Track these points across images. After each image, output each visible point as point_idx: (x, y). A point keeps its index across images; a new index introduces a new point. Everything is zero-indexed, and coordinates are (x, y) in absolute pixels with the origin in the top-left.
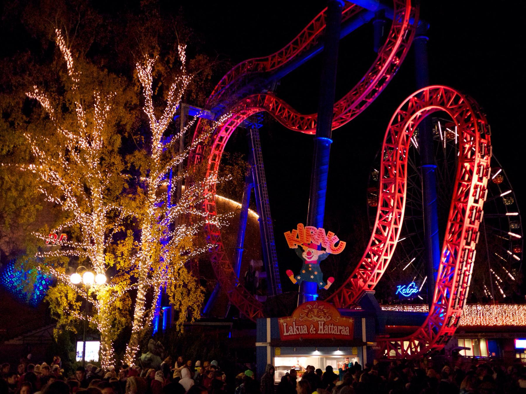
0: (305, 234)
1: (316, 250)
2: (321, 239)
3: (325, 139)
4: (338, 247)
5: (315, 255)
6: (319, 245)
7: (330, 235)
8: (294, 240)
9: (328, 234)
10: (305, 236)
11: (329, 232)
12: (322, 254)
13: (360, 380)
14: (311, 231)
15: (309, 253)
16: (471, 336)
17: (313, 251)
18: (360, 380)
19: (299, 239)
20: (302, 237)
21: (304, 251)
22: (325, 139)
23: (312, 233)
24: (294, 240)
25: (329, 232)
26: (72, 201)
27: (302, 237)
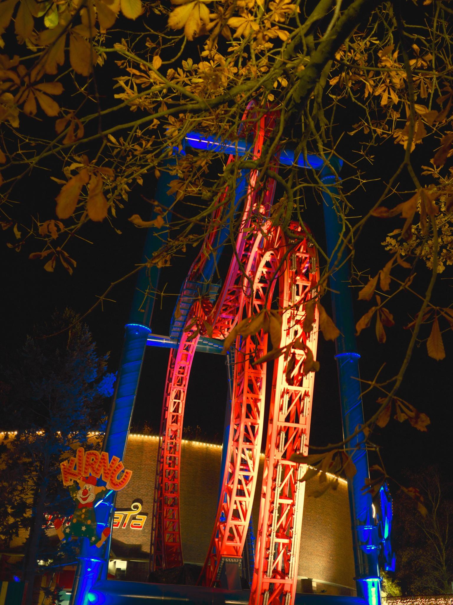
0: (84, 462)
1: (94, 486)
2: (103, 468)
3: (134, 325)
4: (121, 480)
5: (92, 494)
6: (99, 478)
7: (114, 472)
8: (70, 474)
9: (112, 460)
10: (84, 466)
11: (114, 457)
12: (100, 491)
13: (198, 46)
14: (92, 458)
15: (85, 493)
16: (250, 570)
17: (90, 487)
18: (198, 46)
19: (77, 471)
20: (80, 467)
21: (79, 488)
22: (134, 325)
23: (93, 460)
24: (70, 474)
25: (114, 457)
26: (246, 55)
27: (80, 467)
